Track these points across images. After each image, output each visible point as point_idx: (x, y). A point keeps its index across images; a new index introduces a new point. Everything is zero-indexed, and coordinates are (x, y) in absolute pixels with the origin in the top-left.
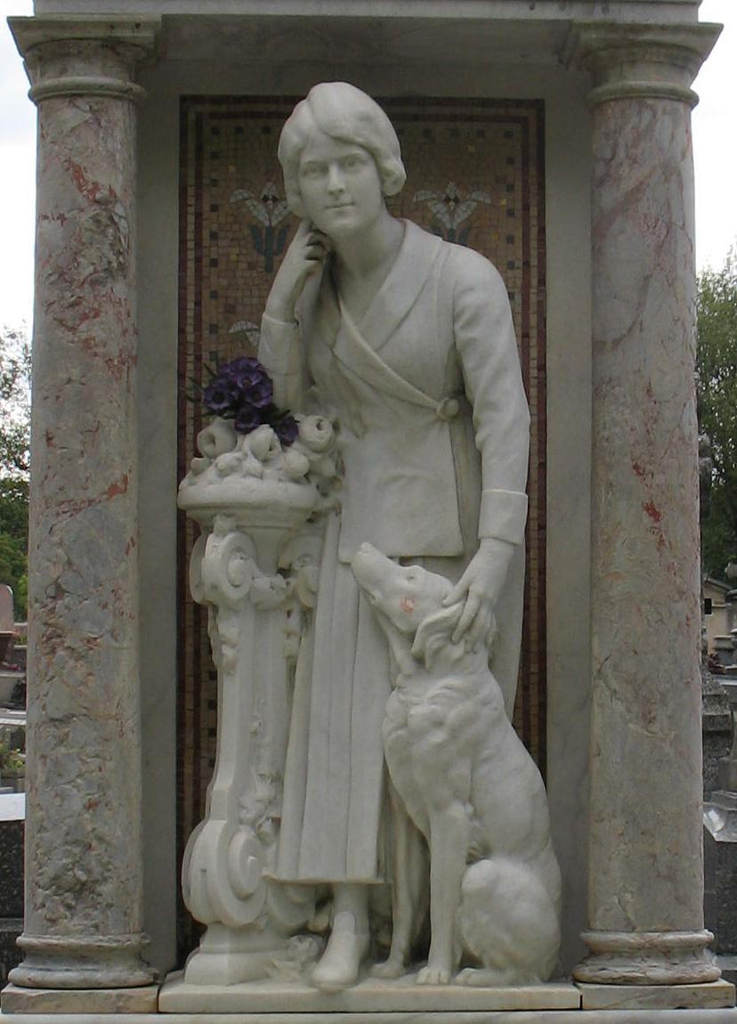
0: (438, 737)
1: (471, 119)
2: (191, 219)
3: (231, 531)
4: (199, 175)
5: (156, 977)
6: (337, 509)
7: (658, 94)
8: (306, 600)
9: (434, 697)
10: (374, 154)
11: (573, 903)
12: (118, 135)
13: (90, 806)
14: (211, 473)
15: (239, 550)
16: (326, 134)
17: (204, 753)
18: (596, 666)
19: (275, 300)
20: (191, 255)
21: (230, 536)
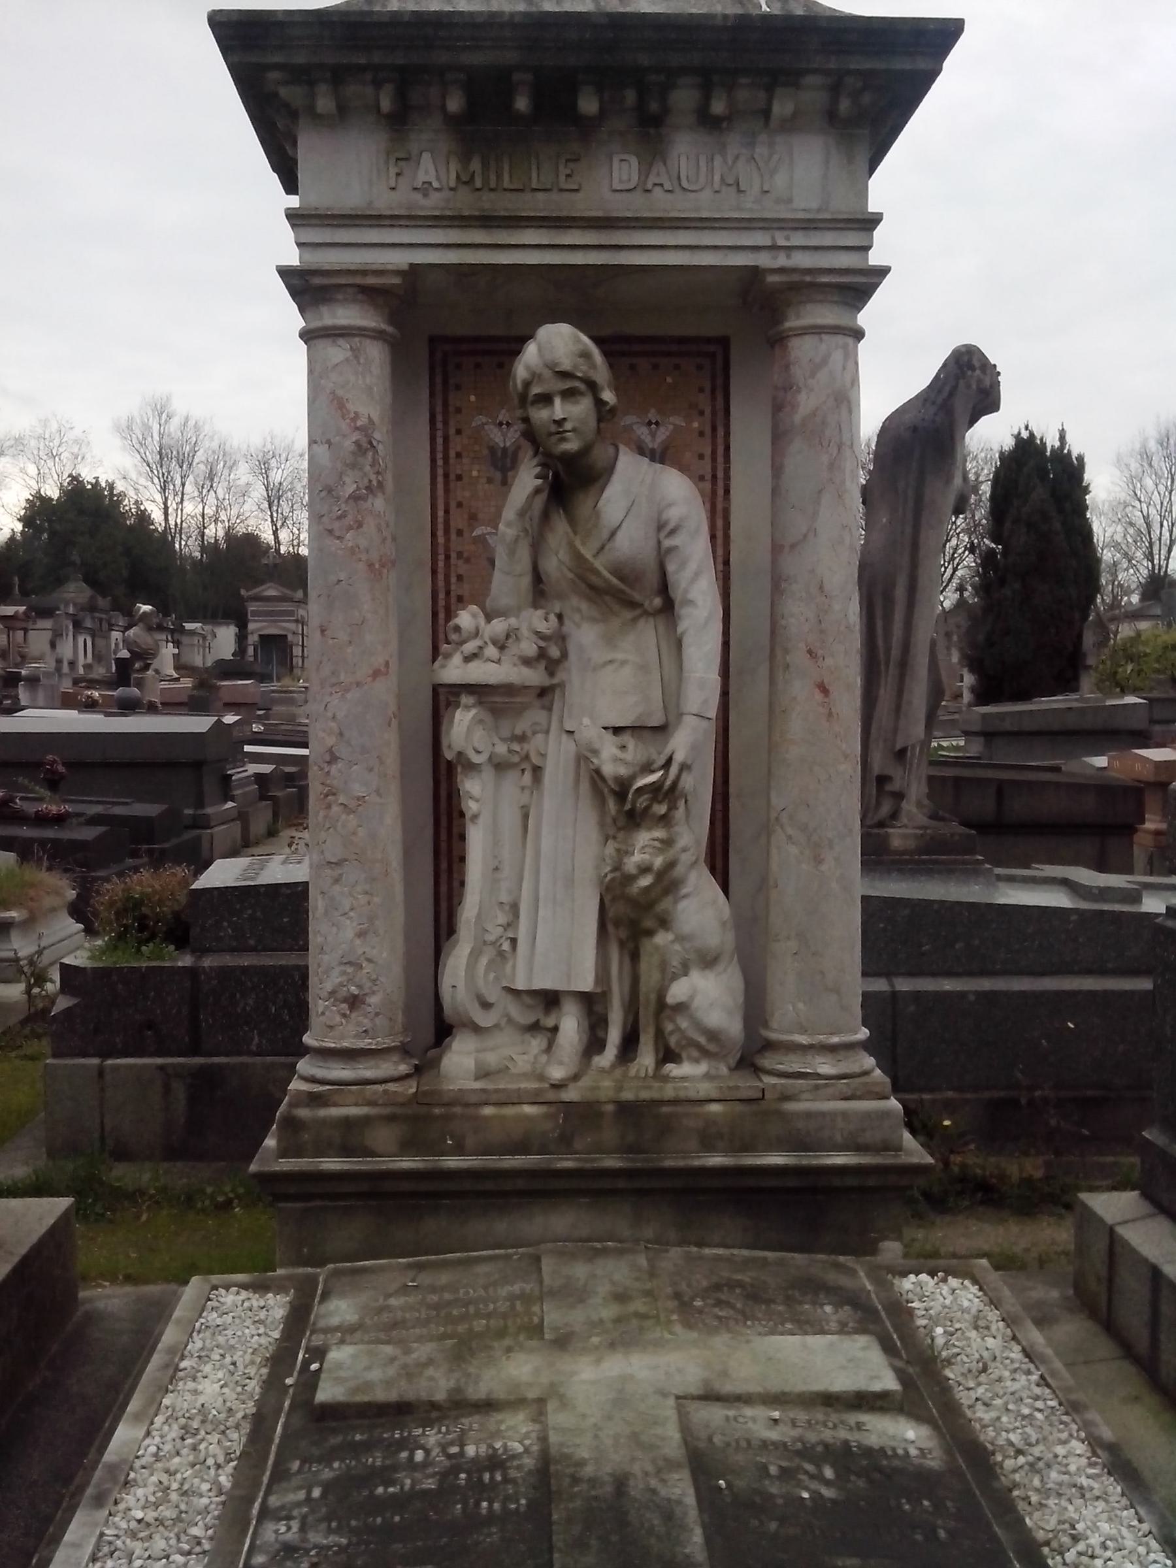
0: (645, 881)
1: (669, 354)
2: (440, 441)
3: (474, 706)
4: (445, 404)
5: (417, 1068)
6: (562, 685)
7: (836, 330)
8: (535, 760)
9: (643, 848)
10: (592, 386)
11: (755, 1006)
12: (376, 370)
13: (361, 934)
14: (457, 659)
15: (481, 721)
16: (550, 369)
17: (455, 875)
18: (773, 815)
19: (509, 513)
20: (440, 471)
21: (473, 711)
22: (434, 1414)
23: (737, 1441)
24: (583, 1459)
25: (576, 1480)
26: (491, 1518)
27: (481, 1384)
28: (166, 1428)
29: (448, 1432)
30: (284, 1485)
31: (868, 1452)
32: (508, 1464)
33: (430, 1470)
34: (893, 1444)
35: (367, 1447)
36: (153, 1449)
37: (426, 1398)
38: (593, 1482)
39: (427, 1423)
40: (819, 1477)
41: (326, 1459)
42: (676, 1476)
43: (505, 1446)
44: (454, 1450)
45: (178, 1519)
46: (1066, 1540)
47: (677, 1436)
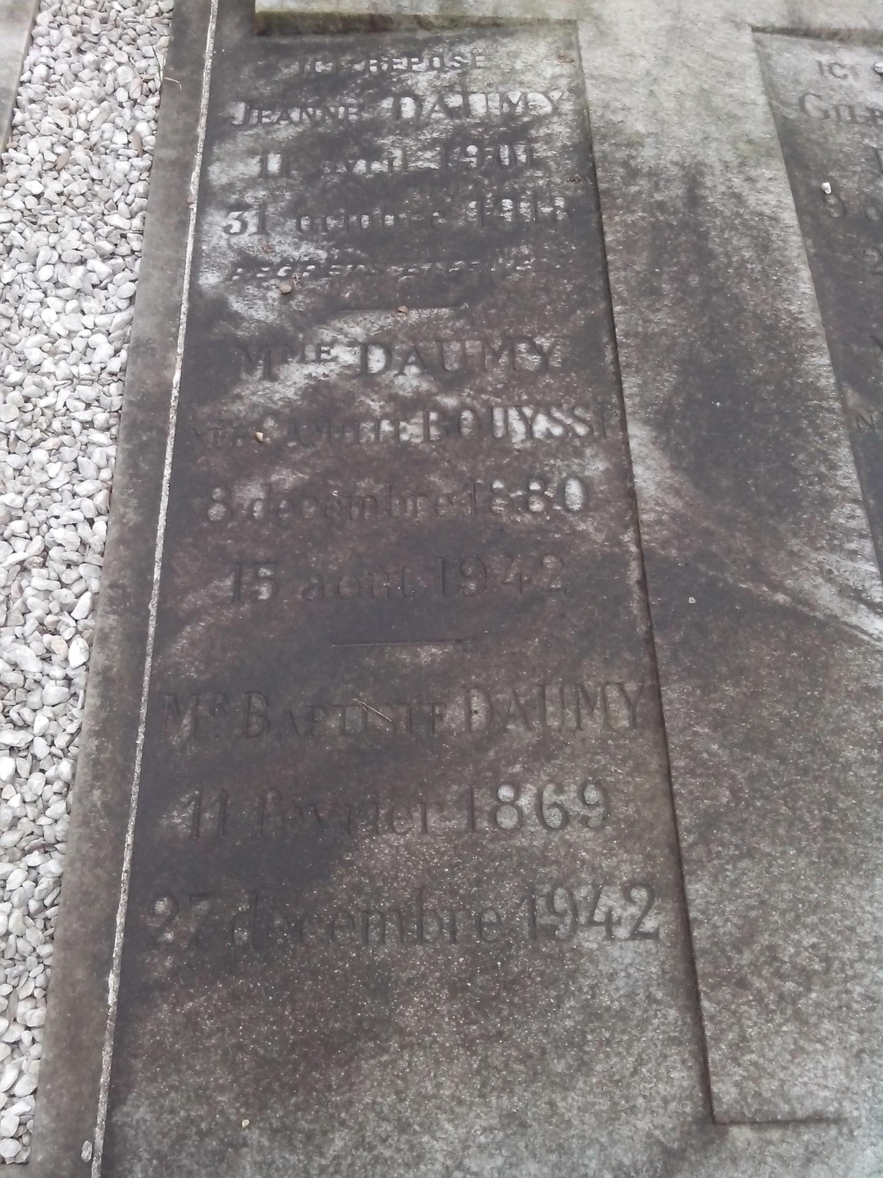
22: (422, 35)
23: (836, 108)
24: (638, 133)
25: (633, 174)
26: (519, 231)
28: (55, 33)
29: (442, 69)
30: (228, 146)
32: (533, 133)
33: (427, 135)
35: (332, 85)
36: (41, 71)
37: (408, 12)
39: (414, 51)
41: (282, 102)
43: (524, 98)
44: (455, 101)
45: (89, 196)
47: (762, 100)
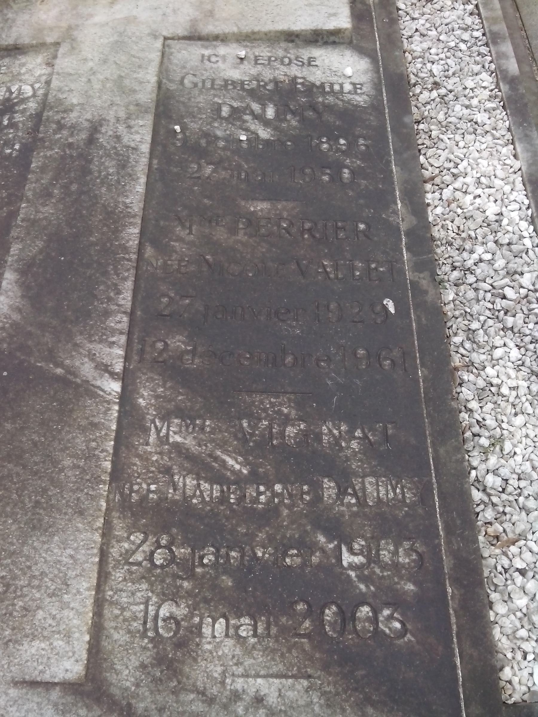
25: (61, 126)
27: (14, 29)
31: (311, 89)
32: (17, 108)
34: (334, 79)
38: (74, 128)
40: (260, 118)
42: (141, 123)
43: (20, 89)
46: (448, 178)
47: (154, 79)
